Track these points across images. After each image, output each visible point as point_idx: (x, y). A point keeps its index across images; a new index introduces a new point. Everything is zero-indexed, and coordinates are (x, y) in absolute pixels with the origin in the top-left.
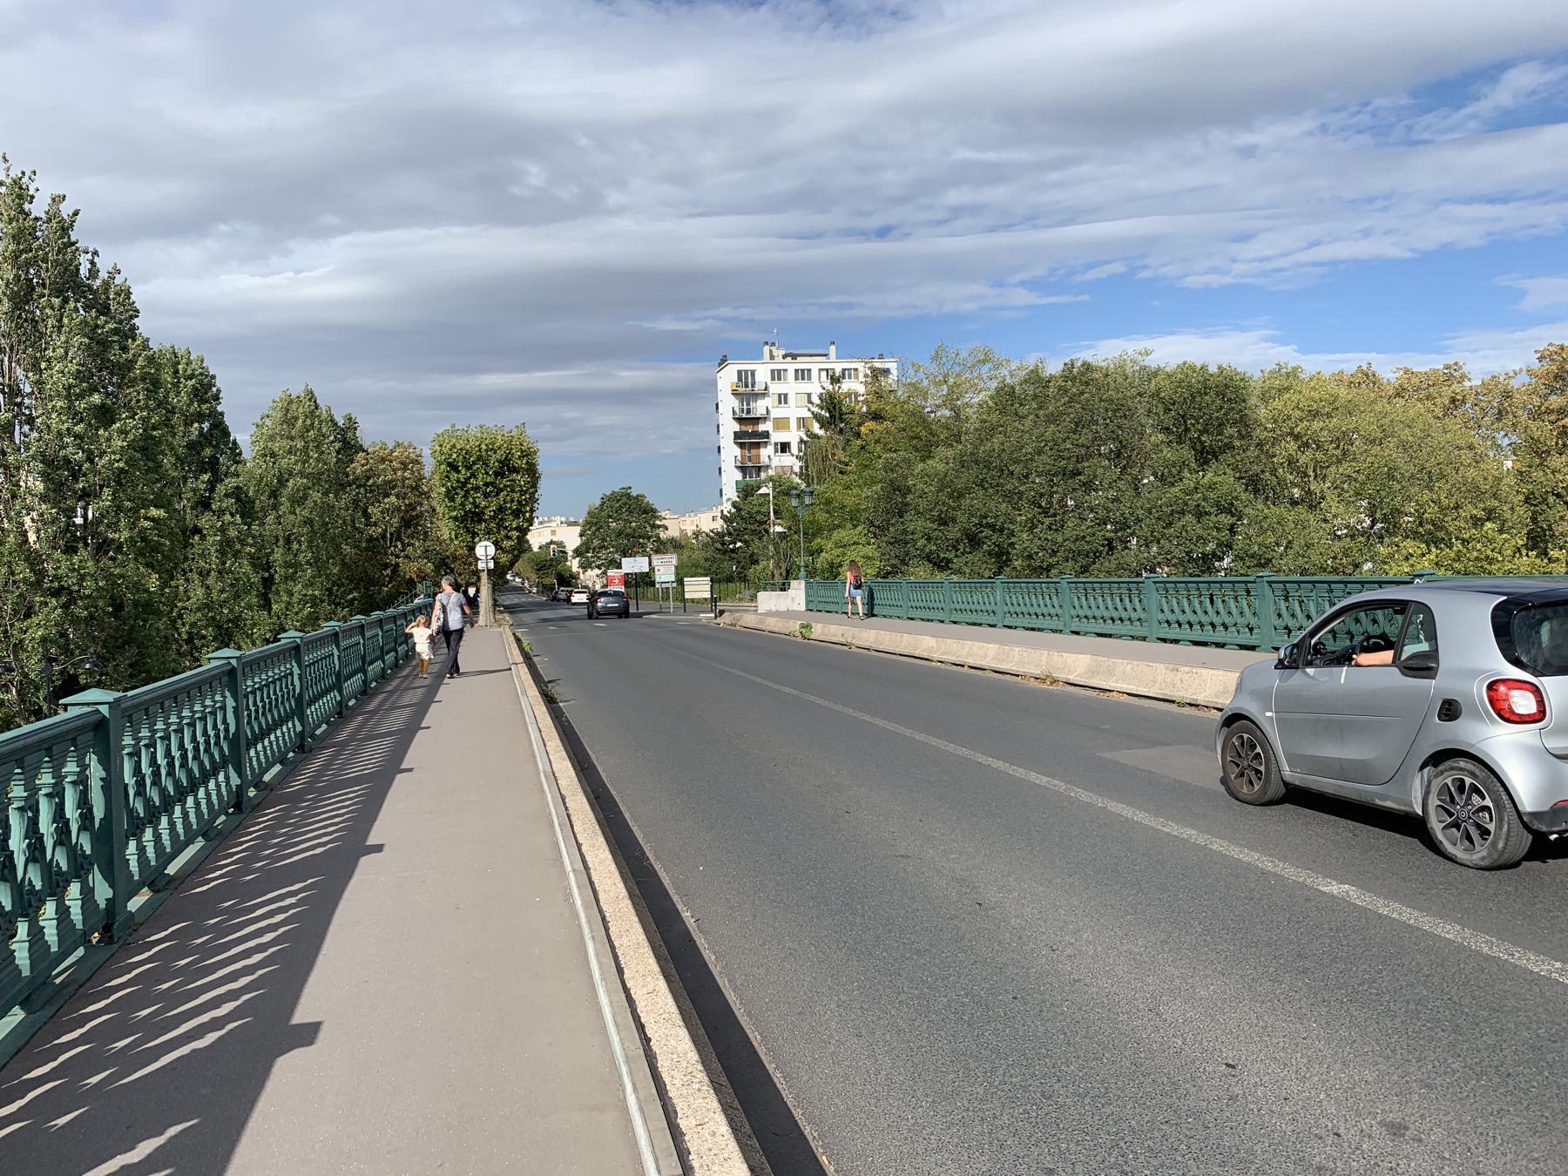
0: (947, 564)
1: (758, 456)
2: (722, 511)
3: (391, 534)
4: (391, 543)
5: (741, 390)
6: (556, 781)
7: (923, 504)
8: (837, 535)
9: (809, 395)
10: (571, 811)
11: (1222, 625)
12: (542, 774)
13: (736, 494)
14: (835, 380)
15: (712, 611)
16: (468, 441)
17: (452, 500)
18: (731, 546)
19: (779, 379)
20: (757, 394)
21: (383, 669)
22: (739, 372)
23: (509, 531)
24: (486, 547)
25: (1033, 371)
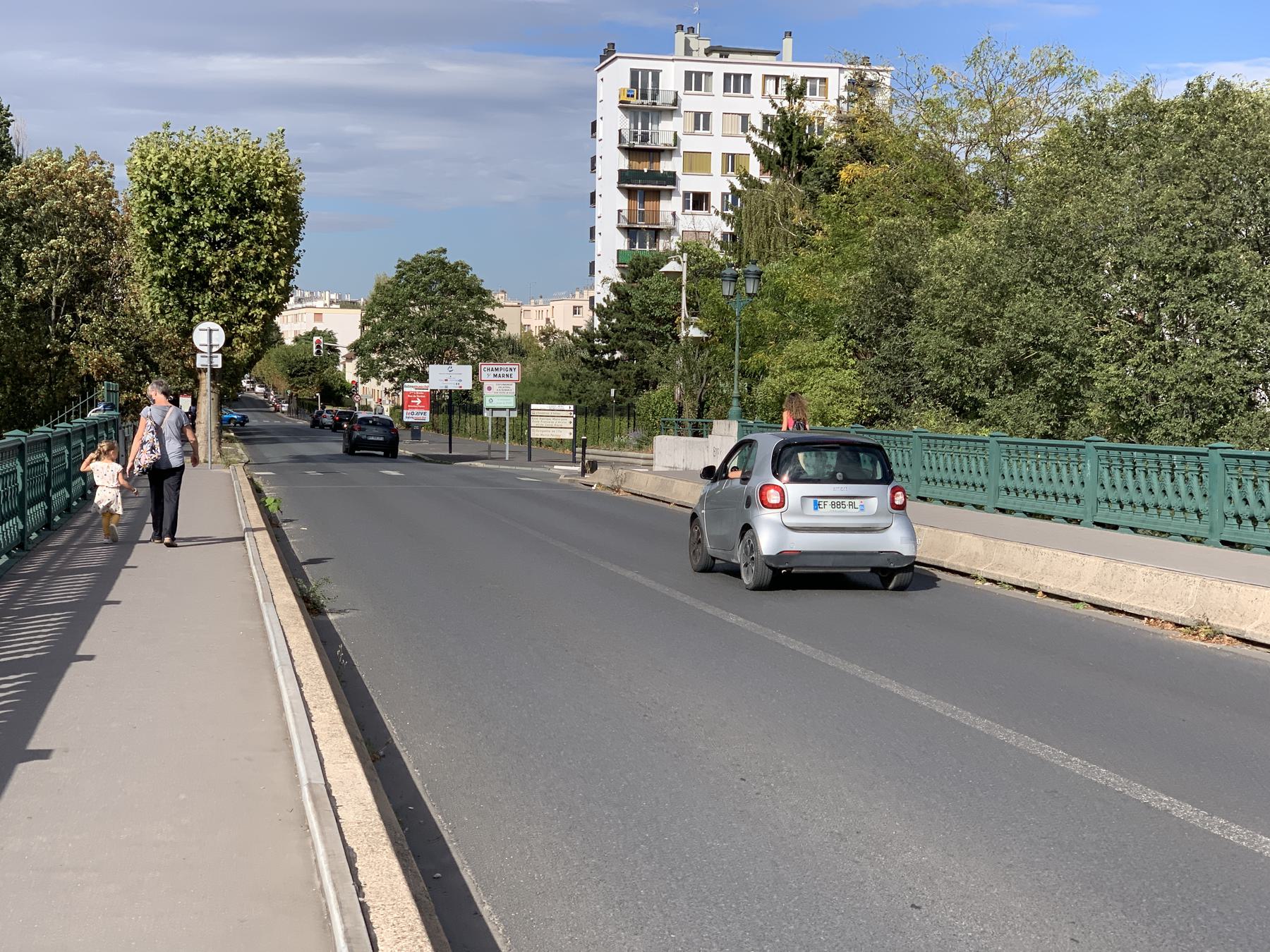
0: (974, 408)
1: (656, 213)
2: (592, 299)
3: (59, 301)
4: (57, 316)
5: (634, 102)
6: (335, 809)
7: (940, 309)
8: (794, 348)
9: (745, 118)
10: (369, 899)
11: (1235, 516)
12: (305, 790)
13: (618, 272)
14: (796, 92)
15: (574, 462)
16: (189, 153)
17: (158, 249)
18: (606, 357)
19: (698, 88)
20: (660, 111)
21: (22, 533)
22: (634, 73)
23: (250, 308)
24: (211, 330)
25: (1139, 92)
